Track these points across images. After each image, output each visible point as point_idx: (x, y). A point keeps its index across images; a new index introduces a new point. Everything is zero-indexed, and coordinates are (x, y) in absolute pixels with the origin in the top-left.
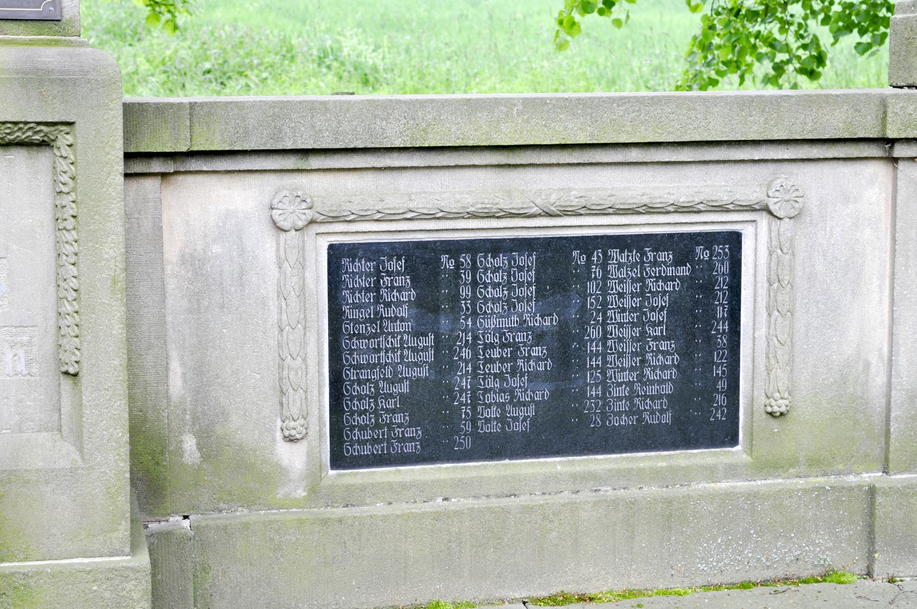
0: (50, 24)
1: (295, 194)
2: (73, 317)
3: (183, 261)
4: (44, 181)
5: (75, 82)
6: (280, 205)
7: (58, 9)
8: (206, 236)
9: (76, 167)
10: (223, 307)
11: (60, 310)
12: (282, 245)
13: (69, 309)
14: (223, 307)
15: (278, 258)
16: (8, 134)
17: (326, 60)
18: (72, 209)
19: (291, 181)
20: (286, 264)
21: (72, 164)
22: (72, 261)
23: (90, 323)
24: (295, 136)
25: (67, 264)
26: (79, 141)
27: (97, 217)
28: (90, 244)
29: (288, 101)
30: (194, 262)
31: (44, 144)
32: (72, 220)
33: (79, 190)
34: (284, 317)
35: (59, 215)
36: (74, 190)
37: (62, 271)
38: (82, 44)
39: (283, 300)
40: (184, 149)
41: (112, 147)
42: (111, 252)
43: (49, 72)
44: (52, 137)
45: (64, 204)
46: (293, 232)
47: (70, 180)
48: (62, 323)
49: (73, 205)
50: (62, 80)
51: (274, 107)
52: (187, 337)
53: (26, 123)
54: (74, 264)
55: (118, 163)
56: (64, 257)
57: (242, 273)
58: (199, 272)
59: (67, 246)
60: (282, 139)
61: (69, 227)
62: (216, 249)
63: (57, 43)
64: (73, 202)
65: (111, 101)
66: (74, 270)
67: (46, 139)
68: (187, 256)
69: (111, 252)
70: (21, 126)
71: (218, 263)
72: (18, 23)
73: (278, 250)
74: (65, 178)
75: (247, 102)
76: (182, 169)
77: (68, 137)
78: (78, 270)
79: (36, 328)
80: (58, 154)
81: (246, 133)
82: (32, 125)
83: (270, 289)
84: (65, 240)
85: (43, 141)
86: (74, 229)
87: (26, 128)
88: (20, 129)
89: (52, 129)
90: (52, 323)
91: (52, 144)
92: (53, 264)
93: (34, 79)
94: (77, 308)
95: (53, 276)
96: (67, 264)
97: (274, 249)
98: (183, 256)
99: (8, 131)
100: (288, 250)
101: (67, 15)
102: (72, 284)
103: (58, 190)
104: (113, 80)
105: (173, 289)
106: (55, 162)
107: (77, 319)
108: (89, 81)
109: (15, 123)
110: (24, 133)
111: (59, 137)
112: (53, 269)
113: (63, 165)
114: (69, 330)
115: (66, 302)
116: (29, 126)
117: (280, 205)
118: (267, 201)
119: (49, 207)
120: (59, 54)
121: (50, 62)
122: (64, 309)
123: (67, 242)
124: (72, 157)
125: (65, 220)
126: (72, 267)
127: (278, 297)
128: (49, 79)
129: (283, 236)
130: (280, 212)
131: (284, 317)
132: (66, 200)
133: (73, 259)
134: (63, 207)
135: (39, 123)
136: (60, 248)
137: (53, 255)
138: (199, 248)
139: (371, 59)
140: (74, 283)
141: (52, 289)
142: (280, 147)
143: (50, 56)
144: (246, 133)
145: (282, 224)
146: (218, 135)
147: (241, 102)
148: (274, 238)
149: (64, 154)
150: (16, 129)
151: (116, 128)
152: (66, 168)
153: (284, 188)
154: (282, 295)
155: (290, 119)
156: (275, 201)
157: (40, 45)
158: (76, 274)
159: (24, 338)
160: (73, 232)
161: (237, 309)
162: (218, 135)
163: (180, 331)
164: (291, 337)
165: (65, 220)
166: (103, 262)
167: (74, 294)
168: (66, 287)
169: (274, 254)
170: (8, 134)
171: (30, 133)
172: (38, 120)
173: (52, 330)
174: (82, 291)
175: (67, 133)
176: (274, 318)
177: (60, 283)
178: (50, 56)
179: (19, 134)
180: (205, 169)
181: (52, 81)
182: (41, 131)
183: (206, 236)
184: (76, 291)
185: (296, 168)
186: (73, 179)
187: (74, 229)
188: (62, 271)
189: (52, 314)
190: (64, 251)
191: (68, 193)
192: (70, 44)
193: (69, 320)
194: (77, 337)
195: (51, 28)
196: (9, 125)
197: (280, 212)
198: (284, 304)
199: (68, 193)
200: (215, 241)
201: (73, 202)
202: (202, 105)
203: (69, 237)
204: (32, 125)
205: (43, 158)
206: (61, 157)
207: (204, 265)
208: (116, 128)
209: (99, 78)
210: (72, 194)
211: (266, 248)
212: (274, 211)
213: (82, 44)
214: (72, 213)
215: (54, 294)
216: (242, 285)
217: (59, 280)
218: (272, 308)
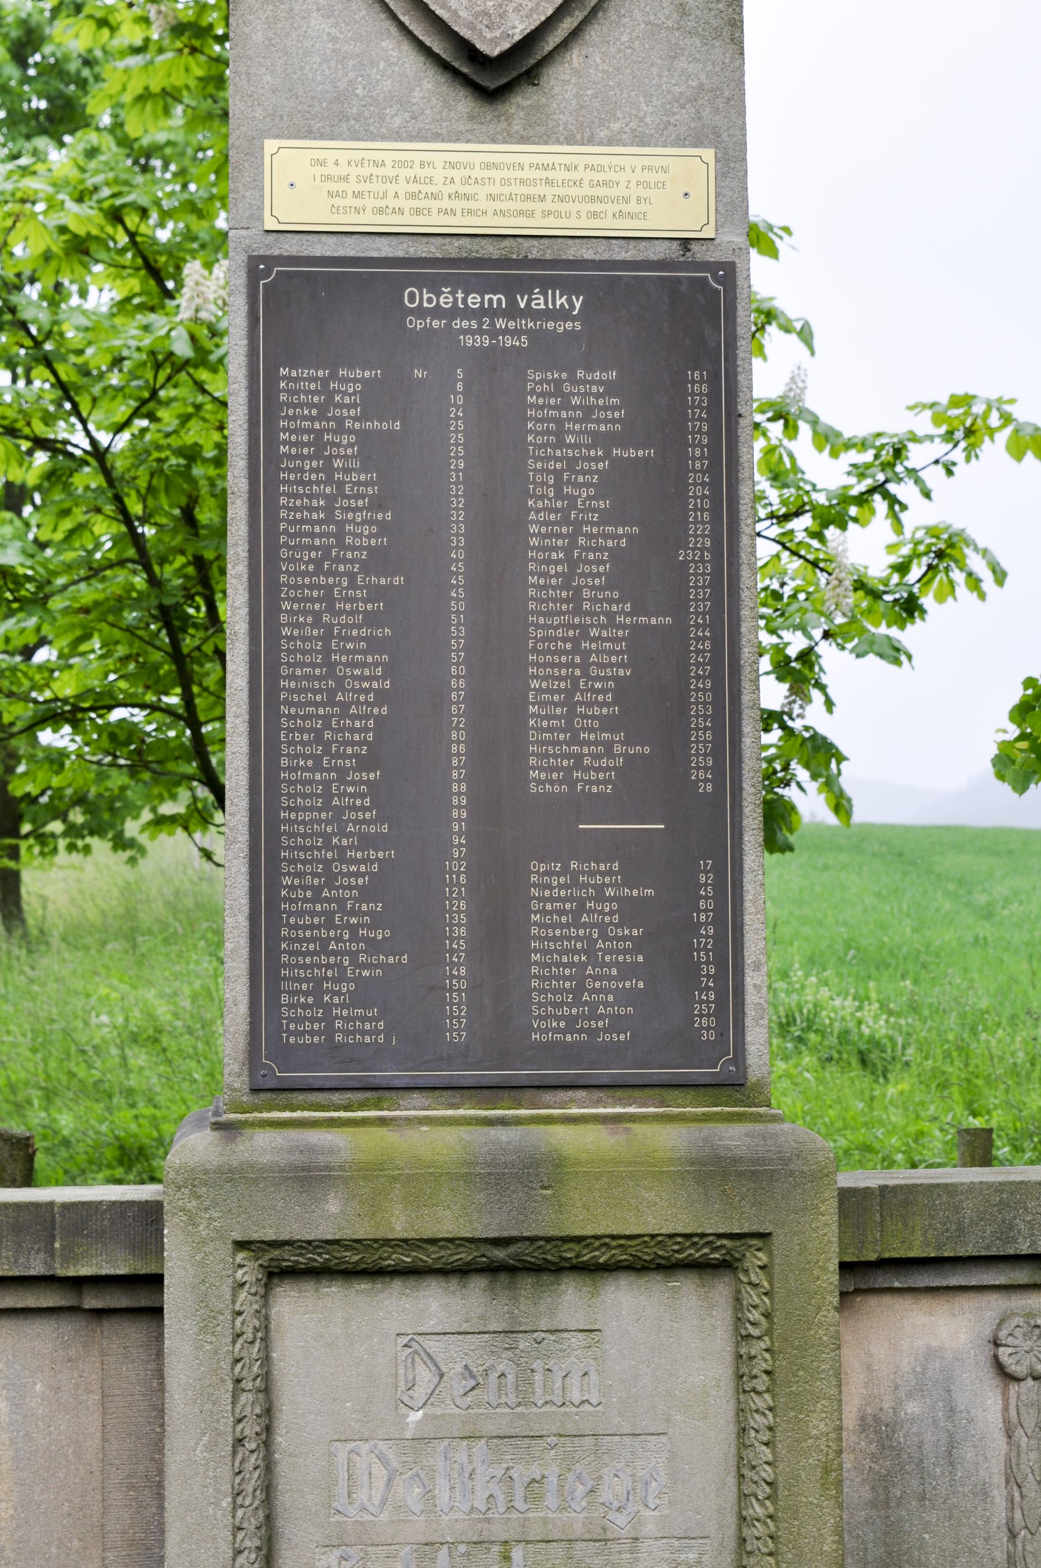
0: (730, 1091)
1: (1033, 1323)
2: (765, 1524)
3: (864, 1425)
4: (722, 1317)
5: (772, 1175)
6: (1010, 1340)
7: (741, 1069)
8: (896, 1388)
9: (771, 1299)
10: (924, 1498)
11: (744, 1513)
12: (1013, 1401)
13: (760, 1511)
14: (924, 1498)
15: (1006, 1421)
16: (677, 1251)
17: (793, 1029)
18: (766, 1360)
19: (1023, 1302)
20: (1019, 1432)
21: (765, 1294)
22: (765, 1439)
23: (791, 1533)
24: (1033, 1235)
25: (757, 1444)
26: (777, 1261)
27: (801, 1373)
28: (792, 1414)
29: (1021, 1182)
30: (881, 1429)
31: (727, 1266)
32: (765, 1377)
33: (776, 1333)
34: (1018, 1515)
35: (744, 1369)
36: (769, 1332)
37: (749, 1454)
38: (775, 1119)
39: (1015, 1488)
40: (873, 1257)
41: (823, 1269)
42: (822, 1425)
43: (736, 1160)
44: (737, 1255)
45: (753, 1352)
46: (1030, 1382)
47: (763, 1320)
48: (746, 1532)
49: (767, 1356)
50: (754, 1173)
51: (1002, 1191)
52: (870, 1545)
53: (703, 1235)
54: (766, 1444)
55: (832, 1292)
56: (753, 1433)
57: (952, 1445)
58: (887, 1443)
59: (756, 1416)
60: (1014, 1240)
61: (761, 1388)
62: (913, 1408)
63: (740, 1118)
64: (767, 1350)
65: (823, 1201)
66: (767, 1453)
67: (728, 1258)
68: (870, 1420)
69: (822, 1425)
70: (696, 1239)
71: (915, 1429)
72: (685, 1089)
73: (1006, 1409)
74: (755, 1315)
75: (962, 1184)
76: (863, 1286)
77: (760, 1254)
78: (774, 1453)
79: (707, 1541)
80: (745, 1279)
81: (961, 1230)
82: (711, 1238)
83: (994, 1472)
84: (754, 1407)
85: (724, 1261)
86: (768, 1391)
87: (702, 1242)
88: (695, 1244)
89: (738, 1243)
90: (731, 1531)
91: (736, 1264)
92: (734, 1443)
93: (713, 1171)
94: (771, 1509)
95: (733, 1461)
96: (757, 1444)
97: (999, 1406)
98: (863, 1418)
99: (676, 1247)
100: (1023, 1410)
101: (754, 1074)
102: (763, 1474)
103: (743, 1332)
104: (825, 1171)
105: (849, 1471)
106: (738, 1291)
107: (772, 1528)
108: (792, 1173)
109: (687, 1236)
110: (698, 1251)
111: (748, 1254)
112: (733, 1450)
113: (752, 1296)
114: (760, 1544)
115: (754, 1501)
116: (706, 1240)
117: (1010, 1340)
118: (987, 1332)
119: (728, 1356)
120: (747, 1135)
121: (736, 1146)
122: (751, 1511)
123: (757, 1411)
124: (766, 1284)
125: (755, 1377)
126: (764, 1448)
127: (1007, 1482)
128: (736, 1171)
129: (1014, 1388)
130: (1010, 1350)
131: (1018, 1515)
132: (757, 1348)
133: (765, 1436)
134: (752, 1358)
135: (720, 1236)
136: (746, 1419)
137: (731, 1429)
138: (886, 1406)
139: (875, 1024)
140: (767, 1473)
141: (731, 1480)
142: (1011, 1252)
143: (735, 1137)
144: (961, 1230)
145: (1014, 1369)
146: (918, 1234)
147: (952, 1184)
148: (999, 1391)
149: (754, 1279)
150: (687, 1244)
151: (829, 1242)
152: (757, 1301)
153: (1014, 1314)
154: (1011, 1478)
155: (1026, 1209)
156: (1002, 1334)
157: (717, 1121)
158: (770, 1458)
159: (691, 1555)
160: (767, 1396)
161: (944, 1503)
162: (918, 1234)
163: (858, 1536)
164: (1029, 1548)
165: (755, 1377)
166: (810, 1441)
167: (768, 1490)
168: (756, 1478)
169: (999, 1415)
170: (677, 1251)
171: (706, 1250)
172: (721, 1231)
173: (731, 1543)
174: (781, 1485)
175: (759, 1250)
176: (1000, 1515)
177: (745, 1471)
178: (735, 1137)
179: (692, 1251)
180: (897, 1284)
181: (740, 1174)
182: (722, 1246)
183: (896, 1388)
184: (768, 1484)
185: (1032, 1281)
186: (767, 1315)
187: (768, 1391)
188: (749, 1454)
189: (732, 1520)
190: (752, 1423)
191: (759, 1338)
192: (758, 1118)
193: (760, 1529)
194: (771, 1554)
195: (730, 1096)
196: (679, 1240)
197: (1010, 1350)
198: (1017, 1494)
199: (759, 1338)
200: (910, 1395)
201: (767, 1350)
202: (896, 1189)
203: (760, 1403)
204: (711, 1238)
205: (721, 1289)
206: (750, 1283)
207: (894, 1432)
208: (829, 1242)
209: (806, 1169)
210: (766, 1338)
211: (986, 1405)
212: (1001, 1350)
213: (775, 1119)
214: (764, 1366)
215: (735, 1489)
216: (951, 1464)
217: (742, 1469)
218: (998, 1500)
